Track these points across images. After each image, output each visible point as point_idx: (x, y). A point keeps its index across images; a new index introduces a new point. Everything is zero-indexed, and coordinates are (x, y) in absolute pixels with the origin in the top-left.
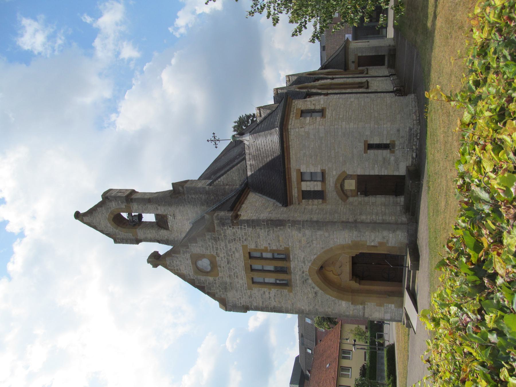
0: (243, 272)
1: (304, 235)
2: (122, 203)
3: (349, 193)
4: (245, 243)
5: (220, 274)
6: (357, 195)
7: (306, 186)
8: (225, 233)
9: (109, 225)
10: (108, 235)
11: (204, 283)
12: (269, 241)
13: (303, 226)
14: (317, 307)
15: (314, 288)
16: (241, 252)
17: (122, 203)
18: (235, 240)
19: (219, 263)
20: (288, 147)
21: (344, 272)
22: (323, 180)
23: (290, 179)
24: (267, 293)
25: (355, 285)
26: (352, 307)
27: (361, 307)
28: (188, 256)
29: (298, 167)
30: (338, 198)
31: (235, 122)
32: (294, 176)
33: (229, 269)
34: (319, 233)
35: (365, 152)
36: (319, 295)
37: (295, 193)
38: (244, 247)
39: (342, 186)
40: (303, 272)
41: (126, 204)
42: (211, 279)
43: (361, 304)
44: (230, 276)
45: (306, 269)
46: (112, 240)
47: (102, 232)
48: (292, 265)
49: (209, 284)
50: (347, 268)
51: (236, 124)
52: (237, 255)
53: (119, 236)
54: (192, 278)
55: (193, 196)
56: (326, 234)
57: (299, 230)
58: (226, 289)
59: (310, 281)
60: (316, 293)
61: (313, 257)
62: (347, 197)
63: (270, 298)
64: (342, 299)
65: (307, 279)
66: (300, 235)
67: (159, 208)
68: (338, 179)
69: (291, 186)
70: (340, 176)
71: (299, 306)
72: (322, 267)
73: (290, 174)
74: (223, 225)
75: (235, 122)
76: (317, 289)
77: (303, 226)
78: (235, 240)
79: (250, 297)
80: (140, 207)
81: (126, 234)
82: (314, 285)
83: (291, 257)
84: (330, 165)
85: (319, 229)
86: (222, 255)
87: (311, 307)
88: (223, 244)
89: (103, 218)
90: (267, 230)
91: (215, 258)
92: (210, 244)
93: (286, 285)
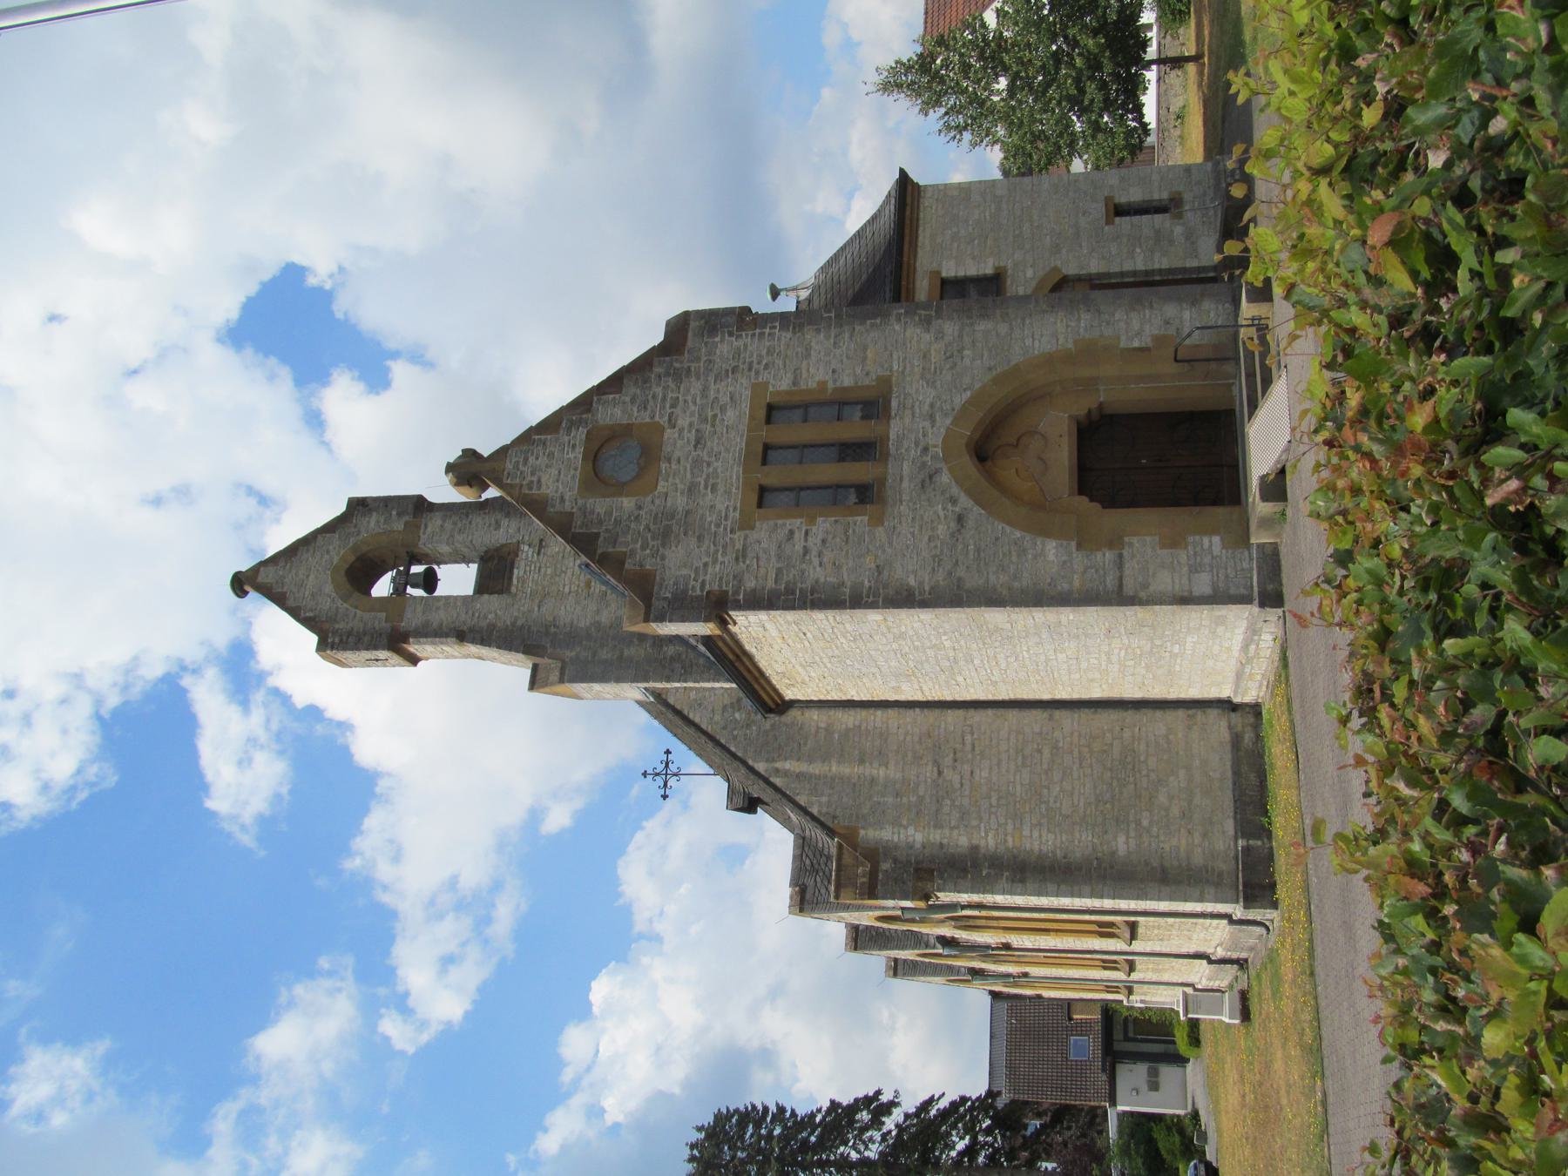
1: (940, 335)
5: (662, 486)
9: (329, 588)
10: (309, 622)
11: (600, 522)
14: (961, 572)
15: (954, 501)
19: (667, 449)
24: (799, 536)
26: (1079, 559)
29: (934, 267)
31: (699, 1129)
33: (697, 463)
34: (982, 326)
35: (1109, 222)
36: (970, 523)
38: (758, 389)
40: (926, 449)
44: (692, 489)
45: (935, 438)
46: (312, 639)
50: (1062, 455)
52: (731, 414)
54: (568, 506)
56: (1003, 329)
58: (665, 536)
59: (945, 478)
60: (960, 519)
61: (960, 399)
63: (806, 551)
64: (1045, 532)
65: (937, 471)
66: (927, 337)
67: (505, 522)
75: (699, 1129)
76: (965, 501)
79: (741, 555)
80: (448, 525)
81: (367, 616)
82: (955, 490)
83: (894, 404)
85: (983, 316)
86: (682, 422)
87: (940, 577)
88: (696, 386)
89: (319, 579)
91: (661, 430)
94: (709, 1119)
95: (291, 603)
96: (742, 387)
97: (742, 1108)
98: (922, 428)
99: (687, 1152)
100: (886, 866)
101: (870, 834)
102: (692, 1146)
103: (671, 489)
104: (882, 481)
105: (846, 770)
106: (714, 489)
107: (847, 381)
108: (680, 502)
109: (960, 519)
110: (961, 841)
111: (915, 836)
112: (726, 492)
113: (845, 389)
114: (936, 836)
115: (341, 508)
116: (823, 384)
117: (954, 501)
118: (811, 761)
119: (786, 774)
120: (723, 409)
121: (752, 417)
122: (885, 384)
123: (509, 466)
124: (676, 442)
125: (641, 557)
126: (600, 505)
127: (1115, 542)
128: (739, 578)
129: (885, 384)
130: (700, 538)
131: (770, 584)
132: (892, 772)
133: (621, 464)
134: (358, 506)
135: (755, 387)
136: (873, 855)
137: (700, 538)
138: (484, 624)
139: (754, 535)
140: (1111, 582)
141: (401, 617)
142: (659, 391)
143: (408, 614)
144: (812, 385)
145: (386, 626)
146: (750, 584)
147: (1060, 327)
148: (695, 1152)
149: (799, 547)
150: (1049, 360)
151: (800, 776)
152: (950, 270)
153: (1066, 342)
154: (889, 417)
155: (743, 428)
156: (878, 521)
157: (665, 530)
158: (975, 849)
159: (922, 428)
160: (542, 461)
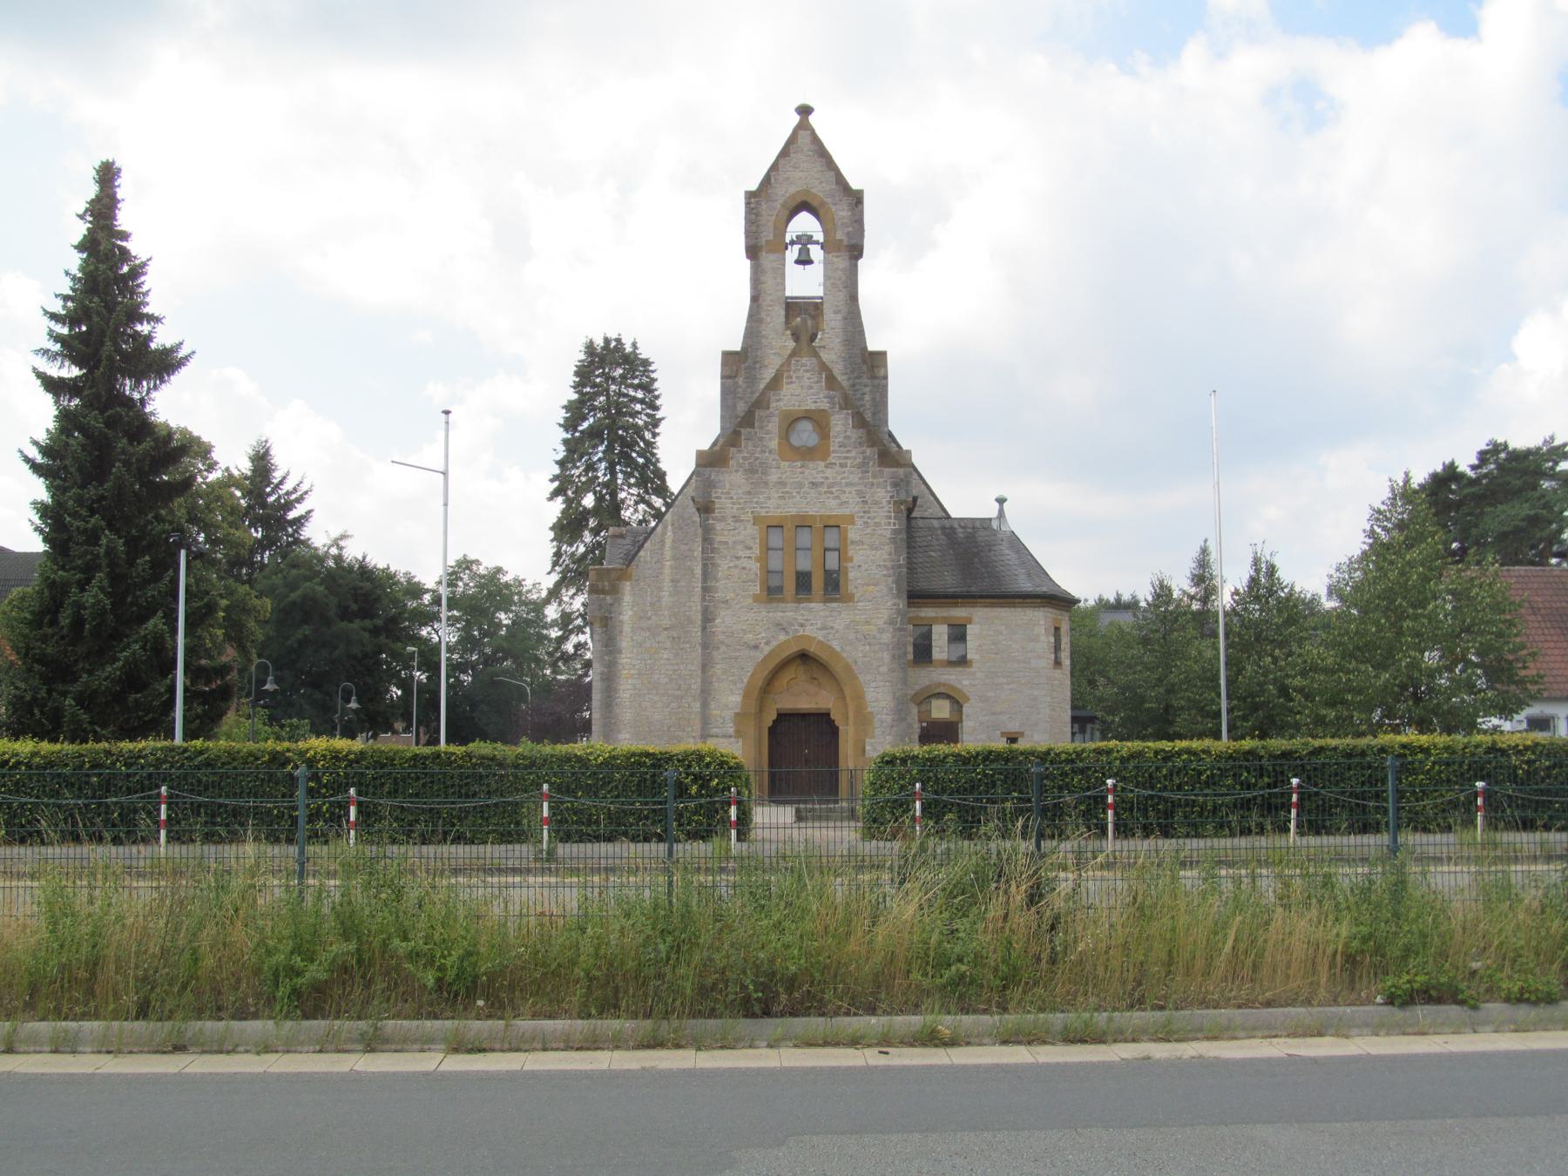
0: (794, 511)
1: (881, 631)
2: (848, 234)
3: (924, 707)
4: (859, 522)
5: (785, 464)
6: (921, 721)
7: (940, 634)
8: (879, 485)
9: (793, 190)
10: (767, 181)
11: (761, 428)
12: (865, 567)
13: (900, 630)
14: (723, 648)
15: (767, 643)
16: (839, 512)
17: (848, 234)
18: (865, 502)
19: (811, 465)
20: (1013, 605)
21: (803, 697)
22: (951, 663)
23: (955, 605)
24: (748, 553)
25: (770, 717)
26: (729, 714)
27: (731, 731)
28: (824, 405)
29: (976, 619)
30: (918, 688)
31: (634, 345)
32: (959, 613)
33: (800, 485)
34: (886, 656)
35: (1003, 734)
36: (752, 653)
37: (928, 612)
38: (850, 519)
39: (939, 695)
40: (802, 625)
41: (846, 242)
42: (774, 444)
43: (737, 731)
44: (782, 484)
45: (809, 631)
46: (754, 187)
47: (774, 167)
48: (816, 606)
49: (761, 439)
50: (805, 704)
51: (628, 349)
52: (833, 503)
53: (764, 206)
54: (773, 405)
55: (867, 397)
56: (884, 669)
57: (891, 622)
58: (751, 471)
59: (782, 637)
60: (756, 647)
61: (836, 645)
62: (919, 704)
63: (738, 558)
64: (746, 695)
65: (787, 633)
66: (881, 622)
67: (839, 317)
68: (954, 688)
69: (940, 606)
70: (959, 691)
71: (722, 613)
72: (804, 657)
73: (963, 605)
74: (895, 485)
75: (634, 345)
76: (767, 650)
77: (900, 630)
78: (865, 502)
79: (736, 519)
80: (839, 273)
81: (771, 224)
82: (774, 643)
83: (834, 605)
84: (979, 675)
85: (894, 656)
86: (829, 473)
87: (721, 637)
88: (855, 478)
89: (804, 178)
90: (889, 564)
91: (824, 459)
92: (853, 454)
93: (772, 593)
94: (644, 353)
95: (782, 162)
96: (853, 508)
97: (656, 385)
98: (816, 623)
99: (613, 335)
100: (609, 599)
101: (627, 587)
102: (618, 341)
103: (783, 471)
104: (782, 601)
105: (667, 571)
106: (781, 498)
107: (851, 575)
108: (774, 477)
109: (756, 647)
110: (624, 643)
111: (627, 615)
112: (774, 505)
113: (846, 574)
114: (627, 628)
115: (854, 186)
116: (851, 559)
117: (767, 643)
118: (673, 548)
119: (664, 534)
120: (837, 497)
121: (830, 517)
122: (849, 598)
123: (804, 360)
124: (815, 470)
125: (737, 457)
126: (774, 426)
127: (739, 734)
128: (723, 519)
129: (849, 598)
130: (749, 493)
131: (719, 538)
132: (666, 599)
133: (805, 435)
134: (857, 198)
135: (852, 516)
136: (615, 590)
137: (749, 493)
138: (763, 314)
139: (749, 526)
140: (714, 731)
141: (770, 251)
142: (853, 454)
143: (771, 257)
144: (850, 553)
145: (763, 242)
146: (719, 526)
147: (883, 704)
148: (613, 344)
149: (740, 553)
150: (859, 696)
151: (662, 542)
152: (971, 630)
153: (872, 707)
154: (825, 602)
155: (823, 512)
156: (756, 599)
157: (755, 471)
158: (620, 652)
159: (816, 623)
160: (806, 382)
